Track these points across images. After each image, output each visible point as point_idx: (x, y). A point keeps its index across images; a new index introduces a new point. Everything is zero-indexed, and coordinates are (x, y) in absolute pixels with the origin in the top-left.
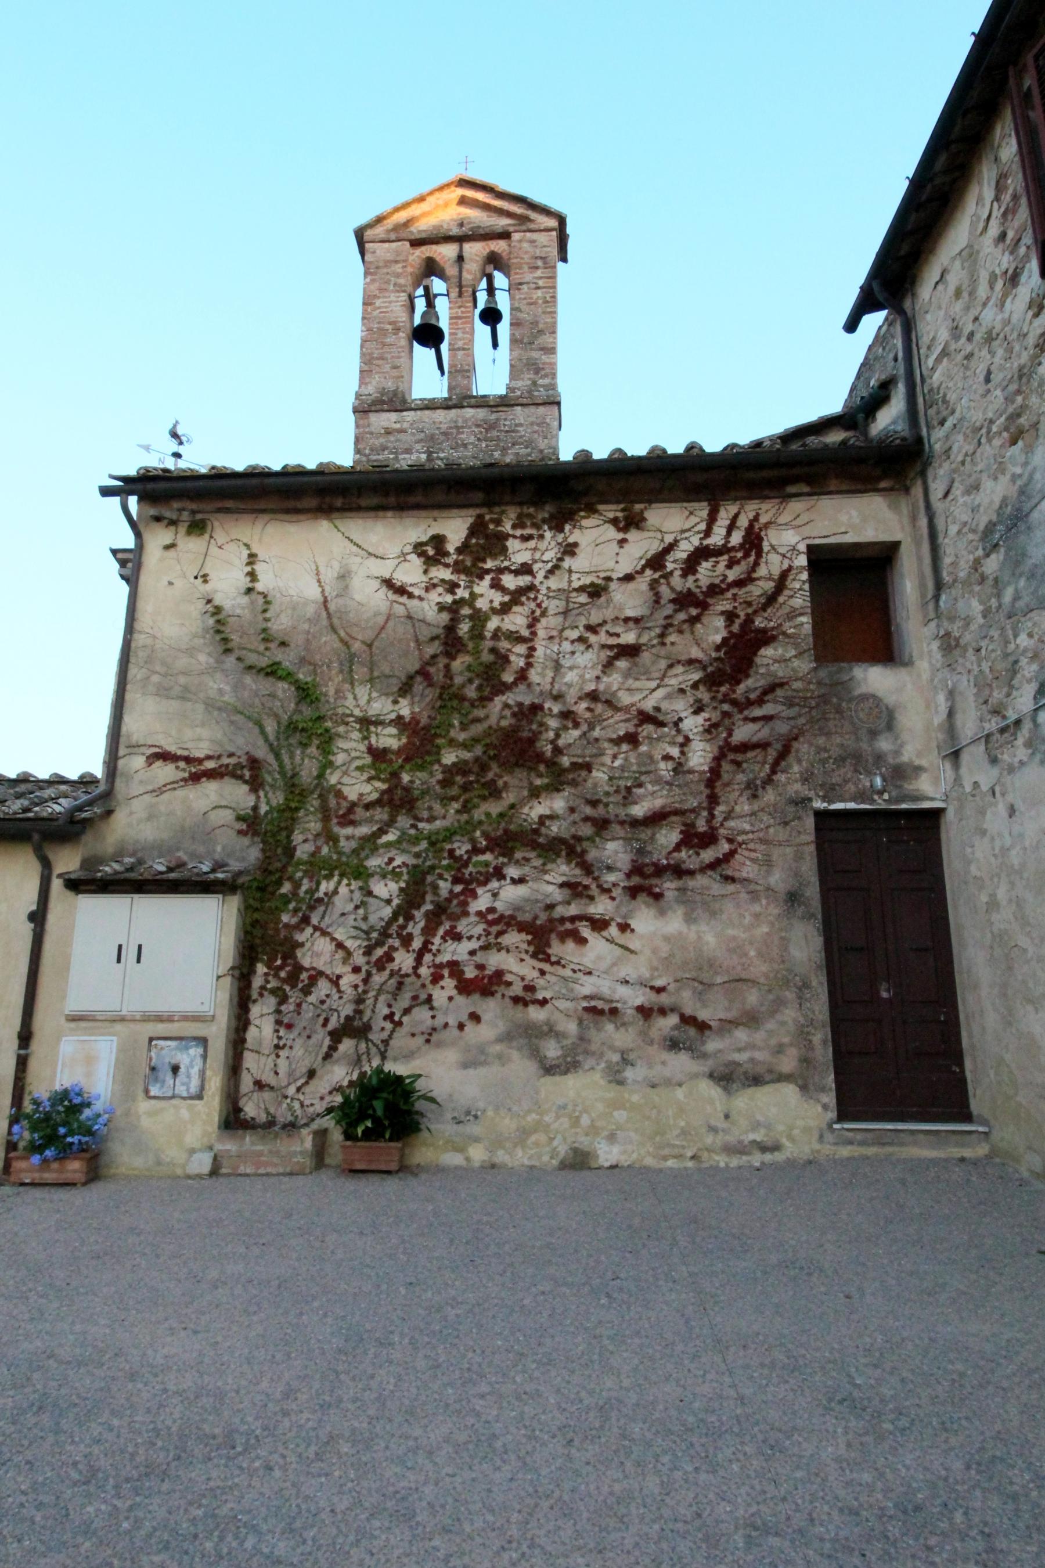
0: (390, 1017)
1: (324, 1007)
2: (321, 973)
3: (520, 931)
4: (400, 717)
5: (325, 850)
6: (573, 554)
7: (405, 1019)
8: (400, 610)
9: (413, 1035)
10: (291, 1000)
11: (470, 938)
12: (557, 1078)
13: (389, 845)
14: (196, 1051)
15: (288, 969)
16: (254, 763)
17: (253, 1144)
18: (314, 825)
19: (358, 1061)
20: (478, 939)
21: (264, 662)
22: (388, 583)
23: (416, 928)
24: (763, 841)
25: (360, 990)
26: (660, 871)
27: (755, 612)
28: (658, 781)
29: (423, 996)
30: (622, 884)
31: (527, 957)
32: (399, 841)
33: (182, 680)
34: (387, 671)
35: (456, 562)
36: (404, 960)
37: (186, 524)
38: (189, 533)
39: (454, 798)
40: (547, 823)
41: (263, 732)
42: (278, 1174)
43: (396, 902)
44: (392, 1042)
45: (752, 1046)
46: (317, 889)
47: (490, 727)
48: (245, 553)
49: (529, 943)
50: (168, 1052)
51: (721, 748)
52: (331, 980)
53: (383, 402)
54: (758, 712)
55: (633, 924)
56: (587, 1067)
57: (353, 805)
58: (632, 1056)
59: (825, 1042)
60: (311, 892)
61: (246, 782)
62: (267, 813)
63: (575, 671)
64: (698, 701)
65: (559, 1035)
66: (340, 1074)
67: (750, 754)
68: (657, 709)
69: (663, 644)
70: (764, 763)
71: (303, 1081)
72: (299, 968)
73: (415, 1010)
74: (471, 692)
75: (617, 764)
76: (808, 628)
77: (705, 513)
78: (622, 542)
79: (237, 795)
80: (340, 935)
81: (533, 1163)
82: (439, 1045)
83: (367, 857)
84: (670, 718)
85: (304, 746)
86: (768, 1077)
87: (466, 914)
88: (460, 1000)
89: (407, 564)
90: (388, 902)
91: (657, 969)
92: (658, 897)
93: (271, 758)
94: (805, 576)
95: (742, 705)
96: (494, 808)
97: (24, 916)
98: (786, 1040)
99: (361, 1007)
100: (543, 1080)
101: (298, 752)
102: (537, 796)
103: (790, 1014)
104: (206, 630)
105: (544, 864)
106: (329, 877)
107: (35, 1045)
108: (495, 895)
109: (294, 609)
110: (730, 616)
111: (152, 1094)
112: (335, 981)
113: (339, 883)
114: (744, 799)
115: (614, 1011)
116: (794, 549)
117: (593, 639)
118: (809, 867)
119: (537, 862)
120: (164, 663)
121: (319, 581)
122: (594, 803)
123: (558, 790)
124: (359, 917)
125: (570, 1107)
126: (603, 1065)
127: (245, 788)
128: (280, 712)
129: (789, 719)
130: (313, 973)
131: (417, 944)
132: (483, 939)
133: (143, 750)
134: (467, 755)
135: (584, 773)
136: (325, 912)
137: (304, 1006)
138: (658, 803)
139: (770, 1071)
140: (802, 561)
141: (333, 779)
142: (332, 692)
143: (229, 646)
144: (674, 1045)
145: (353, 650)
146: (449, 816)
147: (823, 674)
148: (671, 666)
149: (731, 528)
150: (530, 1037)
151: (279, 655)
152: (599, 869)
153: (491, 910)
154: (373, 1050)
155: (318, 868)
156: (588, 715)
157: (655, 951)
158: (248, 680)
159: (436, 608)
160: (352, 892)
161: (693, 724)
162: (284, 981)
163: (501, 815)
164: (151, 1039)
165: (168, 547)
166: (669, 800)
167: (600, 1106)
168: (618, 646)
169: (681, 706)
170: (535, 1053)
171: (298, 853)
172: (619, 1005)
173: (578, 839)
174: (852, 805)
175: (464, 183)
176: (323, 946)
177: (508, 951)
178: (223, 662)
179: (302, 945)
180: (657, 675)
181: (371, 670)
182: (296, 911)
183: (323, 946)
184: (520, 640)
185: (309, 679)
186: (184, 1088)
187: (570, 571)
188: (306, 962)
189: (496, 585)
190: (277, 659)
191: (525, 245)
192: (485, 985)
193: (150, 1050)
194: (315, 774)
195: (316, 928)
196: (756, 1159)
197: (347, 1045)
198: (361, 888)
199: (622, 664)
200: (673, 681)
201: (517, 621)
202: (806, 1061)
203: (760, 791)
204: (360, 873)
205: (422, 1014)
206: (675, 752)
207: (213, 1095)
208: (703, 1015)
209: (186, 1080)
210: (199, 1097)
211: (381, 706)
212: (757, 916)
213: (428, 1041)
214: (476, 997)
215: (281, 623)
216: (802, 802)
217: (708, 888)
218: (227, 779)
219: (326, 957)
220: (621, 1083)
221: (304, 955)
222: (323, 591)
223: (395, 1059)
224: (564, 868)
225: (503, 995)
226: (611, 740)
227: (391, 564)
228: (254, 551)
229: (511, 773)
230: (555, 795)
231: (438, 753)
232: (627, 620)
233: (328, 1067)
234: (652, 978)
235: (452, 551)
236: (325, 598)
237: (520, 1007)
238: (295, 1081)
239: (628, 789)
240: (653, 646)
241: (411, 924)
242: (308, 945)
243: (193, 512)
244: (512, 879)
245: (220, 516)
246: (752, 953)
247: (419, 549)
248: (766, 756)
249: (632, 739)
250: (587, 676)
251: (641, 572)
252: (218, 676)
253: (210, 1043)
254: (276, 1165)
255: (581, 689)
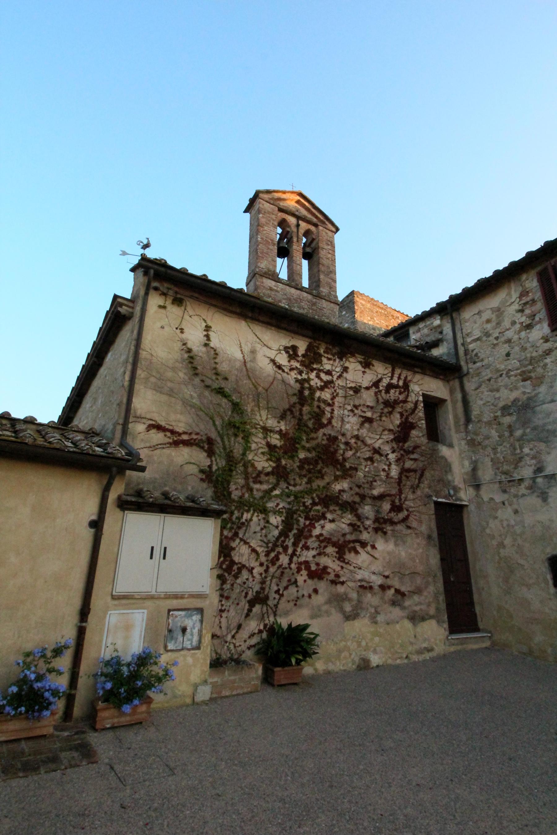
0: (277, 592)
1: (246, 586)
2: (244, 566)
3: (333, 546)
4: (281, 430)
5: (247, 495)
6: (347, 372)
7: (285, 593)
8: (279, 377)
9: (289, 601)
10: (228, 582)
11: (313, 549)
12: (351, 622)
13: (276, 496)
14: (196, 618)
15: (227, 563)
16: (210, 441)
17: (229, 675)
18: (241, 481)
19: (262, 618)
20: (316, 549)
21: (215, 385)
22: (273, 361)
23: (289, 542)
24: (418, 512)
25: (263, 576)
26: (386, 521)
27: (409, 415)
28: (381, 480)
29: (293, 580)
30: (372, 526)
31: (336, 560)
32: (282, 494)
33: (169, 384)
34: (274, 405)
35: (302, 361)
36: (284, 560)
37: (172, 298)
38: (173, 303)
39: (305, 476)
40: (342, 493)
41: (214, 424)
42: (244, 694)
43: (280, 527)
44: (279, 606)
45: (420, 603)
46: (242, 517)
47: (318, 443)
48: (204, 324)
49: (337, 553)
50: (179, 618)
51: (401, 469)
52: (249, 570)
53: (269, 275)
54: (412, 456)
55: (376, 546)
56: (362, 616)
57: (260, 473)
58: (379, 610)
59: (443, 600)
60: (239, 518)
61: (206, 451)
62: (216, 470)
63: (350, 424)
64: (393, 447)
65: (350, 600)
66: (253, 625)
67: (411, 474)
68: (380, 448)
69: (381, 420)
70: (416, 478)
71: (234, 632)
72: (233, 563)
73: (290, 587)
74: (310, 424)
75: (367, 469)
76: (424, 426)
77: (390, 370)
78: (364, 372)
79: (200, 457)
80: (253, 544)
81: (345, 668)
82: (301, 606)
83: (267, 502)
84: (384, 453)
85: (236, 435)
86: (427, 617)
87: (311, 536)
88: (309, 582)
89: (281, 355)
90: (277, 527)
91: (385, 567)
92: (385, 533)
93: (219, 440)
94: (422, 405)
95: (408, 452)
96: (321, 483)
97: (86, 523)
98: (431, 600)
99: (264, 586)
100: (346, 624)
101: (233, 439)
102: (337, 480)
103: (431, 588)
104: (183, 360)
105: (342, 514)
106: (248, 511)
107: (92, 618)
108: (323, 527)
109: (230, 361)
110: (401, 414)
111: (169, 648)
112: (251, 570)
113: (253, 515)
114: (410, 493)
115: (371, 588)
116: (418, 393)
117: (356, 411)
118: (433, 525)
119: (339, 512)
120: (158, 372)
121: (241, 350)
122: (359, 487)
123: (345, 479)
124: (263, 535)
125: (357, 636)
126: (368, 615)
127: (205, 454)
128: (224, 415)
129: (422, 461)
130: (239, 566)
131: (290, 551)
132: (318, 550)
133: (144, 420)
134: (309, 455)
135: (354, 472)
136: (246, 530)
137: (235, 585)
138: (382, 490)
139: (427, 614)
140: (421, 398)
141: (250, 457)
142: (249, 410)
143: (197, 372)
144: (394, 603)
145: (259, 391)
146: (302, 485)
147: (430, 445)
148: (384, 430)
149: (399, 378)
150: (338, 600)
151: (223, 384)
152: (363, 518)
153: (321, 535)
154: (270, 611)
155: (243, 505)
156: (355, 445)
157: (384, 559)
158: (207, 393)
159: (294, 380)
160: (259, 520)
161: (392, 457)
162: (225, 570)
163: (324, 487)
164: (169, 611)
165: (160, 307)
166: (386, 490)
167: (369, 636)
168: (365, 417)
169: (387, 449)
170: (342, 610)
171: (233, 496)
172: (372, 584)
173: (355, 503)
174: (444, 500)
175: (301, 195)
176: (244, 550)
177: (328, 556)
178: (193, 380)
179: (234, 549)
180: (379, 433)
181: (268, 403)
182: (231, 528)
183: (244, 550)
184: (329, 405)
185: (238, 401)
186: (189, 642)
187: (346, 379)
188: (236, 559)
189: (318, 376)
190: (222, 386)
191: (324, 233)
192: (318, 574)
193: (168, 618)
194: (241, 452)
195: (241, 540)
196: (427, 656)
197: (257, 609)
198: (264, 519)
199: (367, 425)
200: (384, 437)
201: (326, 395)
202: (437, 609)
203: (415, 491)
204: (264, 511)
205: (293, 590)
206: (386, 468)
207: (207, 646)
208: (403, 589)
209: (190, 637)
210: (198, 648)
211: (271, 423)
212: (418, 544)
213: (295, 605)
214: (316, 580)
215: (224, 367)
216: (429, 497)
217: (402, 531)
218: (194, 447)
219: (245, 557)
220: (376, 623)
221: (235, 555)
222: (244, 356)
223: (280, 616)
224: (350, 516)
225: (327, 579)
226: (364, 459)
227: (274, 353)
228: (210, 324)
229: (328, 467)
230: (344, 480)
231: (297, 452)
232: (368, 406)
233: (248, 622)
234: (384, 571)
235: (300, 355)
236: (245, 360)
237: (334, 585)
238: (231, 632)
239: (371, 482)
240: (377, 420)
241: (287, 540)
242: (237, 549)
243: (176, 293)
244: (329, 520)
245: (191, 300)
246: (417, 561)
247: (286, 349)
248: (416, 475)
249: (371, 459)
250: (354, 428)
251: (371, 387)
252: (190, 387)
253: (205, 612)
254: (242, 688)
255: (352, 433)
